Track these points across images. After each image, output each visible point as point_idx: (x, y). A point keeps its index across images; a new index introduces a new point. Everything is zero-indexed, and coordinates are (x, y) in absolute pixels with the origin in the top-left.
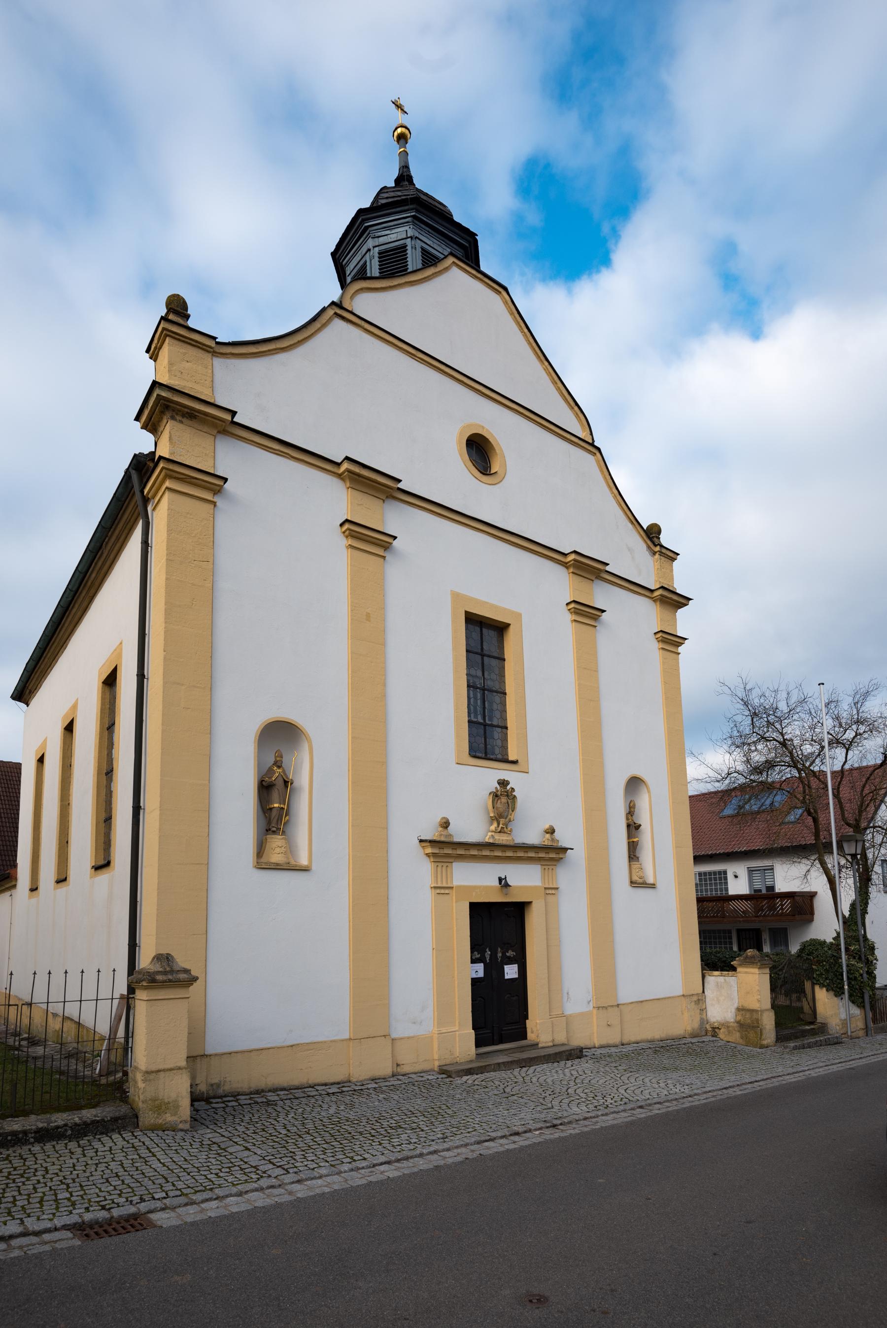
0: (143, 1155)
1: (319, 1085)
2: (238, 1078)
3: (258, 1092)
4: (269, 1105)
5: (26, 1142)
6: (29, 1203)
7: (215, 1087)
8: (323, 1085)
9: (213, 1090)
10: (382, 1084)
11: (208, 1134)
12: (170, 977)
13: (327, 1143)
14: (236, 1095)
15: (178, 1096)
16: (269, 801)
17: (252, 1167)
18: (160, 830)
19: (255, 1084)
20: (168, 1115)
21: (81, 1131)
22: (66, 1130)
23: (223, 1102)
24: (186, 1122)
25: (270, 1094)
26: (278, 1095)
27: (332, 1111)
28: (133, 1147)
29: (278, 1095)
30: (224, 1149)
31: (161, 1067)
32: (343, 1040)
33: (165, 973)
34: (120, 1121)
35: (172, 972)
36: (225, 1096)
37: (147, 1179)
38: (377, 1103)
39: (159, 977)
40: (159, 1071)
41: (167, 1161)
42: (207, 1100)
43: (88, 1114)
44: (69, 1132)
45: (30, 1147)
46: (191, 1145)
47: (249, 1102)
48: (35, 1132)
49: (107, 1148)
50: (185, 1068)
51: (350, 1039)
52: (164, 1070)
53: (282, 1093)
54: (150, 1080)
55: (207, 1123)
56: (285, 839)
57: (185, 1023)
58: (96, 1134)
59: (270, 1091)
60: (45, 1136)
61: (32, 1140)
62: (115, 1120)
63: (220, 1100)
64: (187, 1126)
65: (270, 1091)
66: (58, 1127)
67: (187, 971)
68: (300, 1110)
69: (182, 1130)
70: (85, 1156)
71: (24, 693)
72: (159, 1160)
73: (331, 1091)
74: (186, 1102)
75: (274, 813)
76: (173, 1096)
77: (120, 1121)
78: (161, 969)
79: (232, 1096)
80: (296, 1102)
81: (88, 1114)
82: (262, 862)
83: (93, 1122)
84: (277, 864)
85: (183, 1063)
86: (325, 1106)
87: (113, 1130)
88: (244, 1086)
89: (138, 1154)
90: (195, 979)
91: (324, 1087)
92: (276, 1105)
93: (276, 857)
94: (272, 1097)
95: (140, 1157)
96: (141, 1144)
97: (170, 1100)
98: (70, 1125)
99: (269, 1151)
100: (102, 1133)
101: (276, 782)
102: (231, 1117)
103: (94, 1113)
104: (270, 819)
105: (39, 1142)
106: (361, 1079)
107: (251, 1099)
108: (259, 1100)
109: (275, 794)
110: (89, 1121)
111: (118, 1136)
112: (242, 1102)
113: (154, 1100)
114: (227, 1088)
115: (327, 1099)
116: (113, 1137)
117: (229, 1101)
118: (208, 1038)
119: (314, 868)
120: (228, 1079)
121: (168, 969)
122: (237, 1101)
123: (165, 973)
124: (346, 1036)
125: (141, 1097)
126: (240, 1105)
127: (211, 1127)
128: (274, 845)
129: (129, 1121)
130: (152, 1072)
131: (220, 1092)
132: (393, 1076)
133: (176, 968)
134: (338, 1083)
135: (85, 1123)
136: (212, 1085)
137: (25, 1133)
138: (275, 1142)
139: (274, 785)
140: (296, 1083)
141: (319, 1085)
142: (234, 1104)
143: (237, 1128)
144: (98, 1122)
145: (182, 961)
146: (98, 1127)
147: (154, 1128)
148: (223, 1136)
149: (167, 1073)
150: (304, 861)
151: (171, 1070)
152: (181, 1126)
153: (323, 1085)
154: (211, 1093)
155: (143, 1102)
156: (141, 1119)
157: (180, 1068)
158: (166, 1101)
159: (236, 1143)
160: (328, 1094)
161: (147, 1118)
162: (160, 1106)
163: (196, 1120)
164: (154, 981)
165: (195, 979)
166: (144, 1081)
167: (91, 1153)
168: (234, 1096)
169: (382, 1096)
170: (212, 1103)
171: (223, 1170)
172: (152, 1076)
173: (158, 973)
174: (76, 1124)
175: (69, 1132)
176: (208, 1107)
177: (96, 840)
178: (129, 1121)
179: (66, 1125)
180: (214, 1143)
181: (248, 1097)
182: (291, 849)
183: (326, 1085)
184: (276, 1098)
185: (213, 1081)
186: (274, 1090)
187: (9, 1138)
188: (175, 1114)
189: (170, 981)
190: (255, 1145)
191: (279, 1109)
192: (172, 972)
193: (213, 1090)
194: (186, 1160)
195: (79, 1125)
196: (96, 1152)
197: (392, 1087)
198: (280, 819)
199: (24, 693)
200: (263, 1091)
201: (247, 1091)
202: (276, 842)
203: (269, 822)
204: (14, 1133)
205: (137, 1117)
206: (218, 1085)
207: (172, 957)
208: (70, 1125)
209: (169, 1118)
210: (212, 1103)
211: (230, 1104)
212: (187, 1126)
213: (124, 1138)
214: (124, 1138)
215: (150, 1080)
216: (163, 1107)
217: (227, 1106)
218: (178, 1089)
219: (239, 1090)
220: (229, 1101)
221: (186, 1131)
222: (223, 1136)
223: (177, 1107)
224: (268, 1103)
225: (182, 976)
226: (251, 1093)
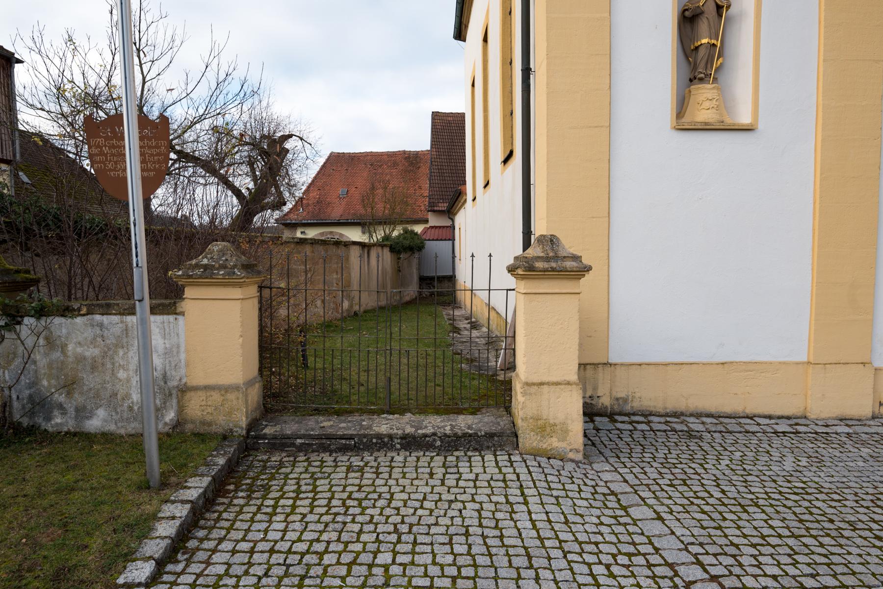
0: (512, 499)
1: (760, 416)
2: (649, 394)
3: (676, 415)
4: (691, 437)
5: (392, 448)
6: (405, 506)
7: (621, 402)
8: (765, 417)
9: (619, 405)
10: (858, 429)
11: (605, 472)
12: (554, 265)
13: (793, 536)
14: (647, 414)
15: (566, 418)
16: (694, 37)
17: (667, 564)
18: (548, 84)
19: (671, 406)
20: (554, 439)
21: (452, 443)
22: (434, 440)
23: (631, 423)
24: (577, 451)
25: (692, 419)
26: (703, 423)
27: (789, 464)
28: (504, 481)
29: (703, 423)
30: (624, 508)
31: (545, 379)
32: (797, 363)
33: (547, 259)
34: (496, 438)
35: (556, 258)
36: (634, 414)
37: (503, 551)
38: (861, 464)
39: (539, 265)
40: (542, 384)
41: (539, 517)
42: (611, 416)
43: (464, 423)
44: (438, 443)
45: (394, 454)
46: (580, 491)
47: (664, 427)
48: (401, 438)
49: (472, 476)
50: (577, 384)
51: (809, 363)
52: (548, 384)
53: (708, 420)
54: (531, 394)
55: (607, 453)
56: (718, 89)
57: (575, 326)
58: (468, 450)
59: (691, 415)
60: (412, 443)
61: (398, 446)
62: (490, 436)
63: (626, 419)
64: (579, 457)
65: (691, 415)
66: (425, 436)
67: (576, 258)
68: (738, 454)
69: (572, 461)
70: (443, 484)
71: (460, 34)
72: (530, 513)
73: (780, 428)
74: (577, 425)
75: (702, 52)
76: (561, 417)
77: (496, 438)
78: (542, 255)
79: (642, 415)
80: (730, 439)
81: (464, 423)
82: (683, 121)
83: (465, 435)
84: (706, 124)
85: (574, 377)
86: (776, 455)
87: (488, 448)
88: (659, 407)
89: (506, 496)
90: (588, 269)
91: (767, 421)
92: (701, 438)
93: (703, 113)
94: (695, 425)
95: (508, 502)
96: (514, 477)
97: (557, 422)
98: (439, 435)
99: (696, 531)
100: (475, 450)
101: (705, 9)
102: (639, 449)
103: (470, 422)
104: (695, 64)
105: (406, 450)
106: (823, 416)
107: (666, 422)
108: (678, 427)
109: (703, 26)
110: (460, 433)
111: (492, 457)
112: (656, 427)
113: (537, 419)
114: (636, 405)
115: (776, 442)
116: (486, 458)
117: (638, 422)
118: (612, 343)
119: (761, 126)
120: (637, 395)
121: (551, 254)
122: (648, 423)
123: (547, 259)
124: (805, 359)
125: (521, 413)
126: (652, 430)
127: (612, 460)
128: (701, 98)
129: (505, 440)
130: (534, 384)
131: (628, 408)
132: (874, 418)
133: (562, 253)
134: (788, 418)
135: (455, 435)
136: (617, 399)
137: (391, 437)
138: (703, 512)
139: (702, 13)
140: (728, 409)
141: (760, 416)
142: (644, 427)
143: (647, 469)
144: (470, 435)
145: (570, 245)
146: (470, 442)
147: (536, 454)
148: (626, 481)
149: (553, 388)
150: (744, 118)
151: (557, 384)
152: (571, 455)
153: (765, 417)
154: (616, 408)
155: (522, 420)
156: (520, 440)
157: (569, 383)
158: (552, 422)
159: (643, 499)
160: (776, 432)
161: (528, 439)
162: (544, 428)
163: (592, 443)
164: (531, 268)
165: (588, 269)
166: (524, 394)
167: (451, 481)
168: (645, 416)
169: (865, 451)
170: (616, 421)
171: (619, 558)
172: (534, 389)
173: (538, 258)
174: (445, 435)
175: (438, 443)
176: (610, 426)
177: (504, 135)
178: (505, 440)
179: (434, 434)
180: (613, 493)
181: (662, 420)
182: (725, 102)
183: (770, 417)
184: (701, 427)
185: (619, 395)
186: (698, 415)
187: (374, 441)
188: (563, 439)
189: (553, 269)
190: (671, 513)
191: (707, 447)
192: (556, 258)
193: (619, 405)
194: (566, 522)
195: (449, 437)
196: (458, 480)
197: (877, 438)
198: (709, 61)
199: (460, 34)
200: (682, 414)
201: (662, 411)
202: (704, 93)
203: (694, 67)
204: (379, 436)
205: (517, 437)
206: (625, 400)
207: (558, 239)
208: (439, 435)
209: (555, 443)
210: (616, 421)
211: (640, 427)
212: (579, 457)
213: (497, 462)
214: (497, 462)
215: (531, 394)
216: (548, 429)
217: (635, 429)
218: (568, 409)
219: (652, 409)
220: (638, 422)
221: (577, 463)
222: (626, 481)
223: (566, 432)
224: (690, 434)
225: (569, 264)
226: (667, 415)
